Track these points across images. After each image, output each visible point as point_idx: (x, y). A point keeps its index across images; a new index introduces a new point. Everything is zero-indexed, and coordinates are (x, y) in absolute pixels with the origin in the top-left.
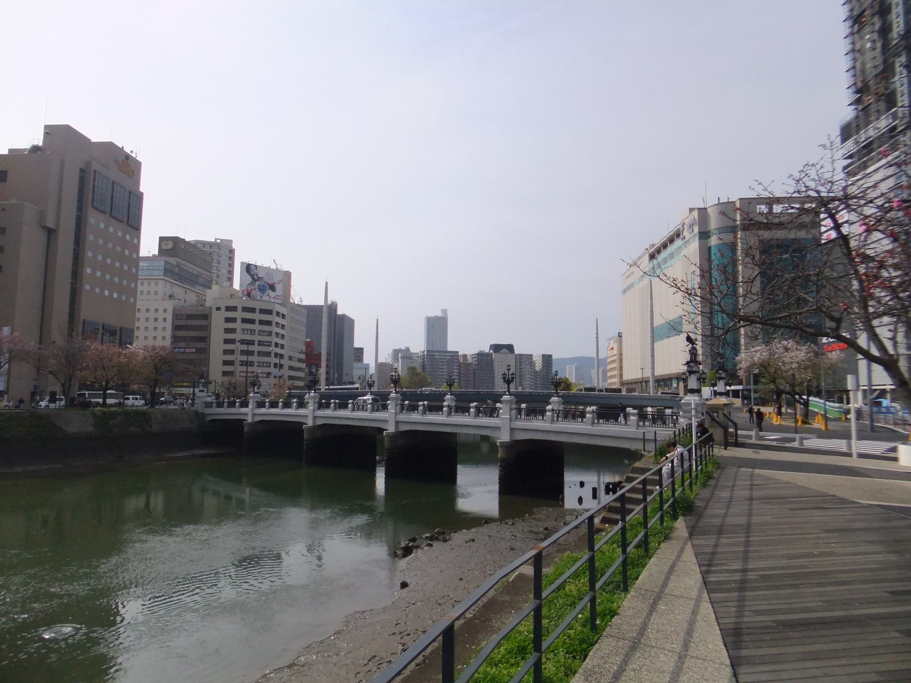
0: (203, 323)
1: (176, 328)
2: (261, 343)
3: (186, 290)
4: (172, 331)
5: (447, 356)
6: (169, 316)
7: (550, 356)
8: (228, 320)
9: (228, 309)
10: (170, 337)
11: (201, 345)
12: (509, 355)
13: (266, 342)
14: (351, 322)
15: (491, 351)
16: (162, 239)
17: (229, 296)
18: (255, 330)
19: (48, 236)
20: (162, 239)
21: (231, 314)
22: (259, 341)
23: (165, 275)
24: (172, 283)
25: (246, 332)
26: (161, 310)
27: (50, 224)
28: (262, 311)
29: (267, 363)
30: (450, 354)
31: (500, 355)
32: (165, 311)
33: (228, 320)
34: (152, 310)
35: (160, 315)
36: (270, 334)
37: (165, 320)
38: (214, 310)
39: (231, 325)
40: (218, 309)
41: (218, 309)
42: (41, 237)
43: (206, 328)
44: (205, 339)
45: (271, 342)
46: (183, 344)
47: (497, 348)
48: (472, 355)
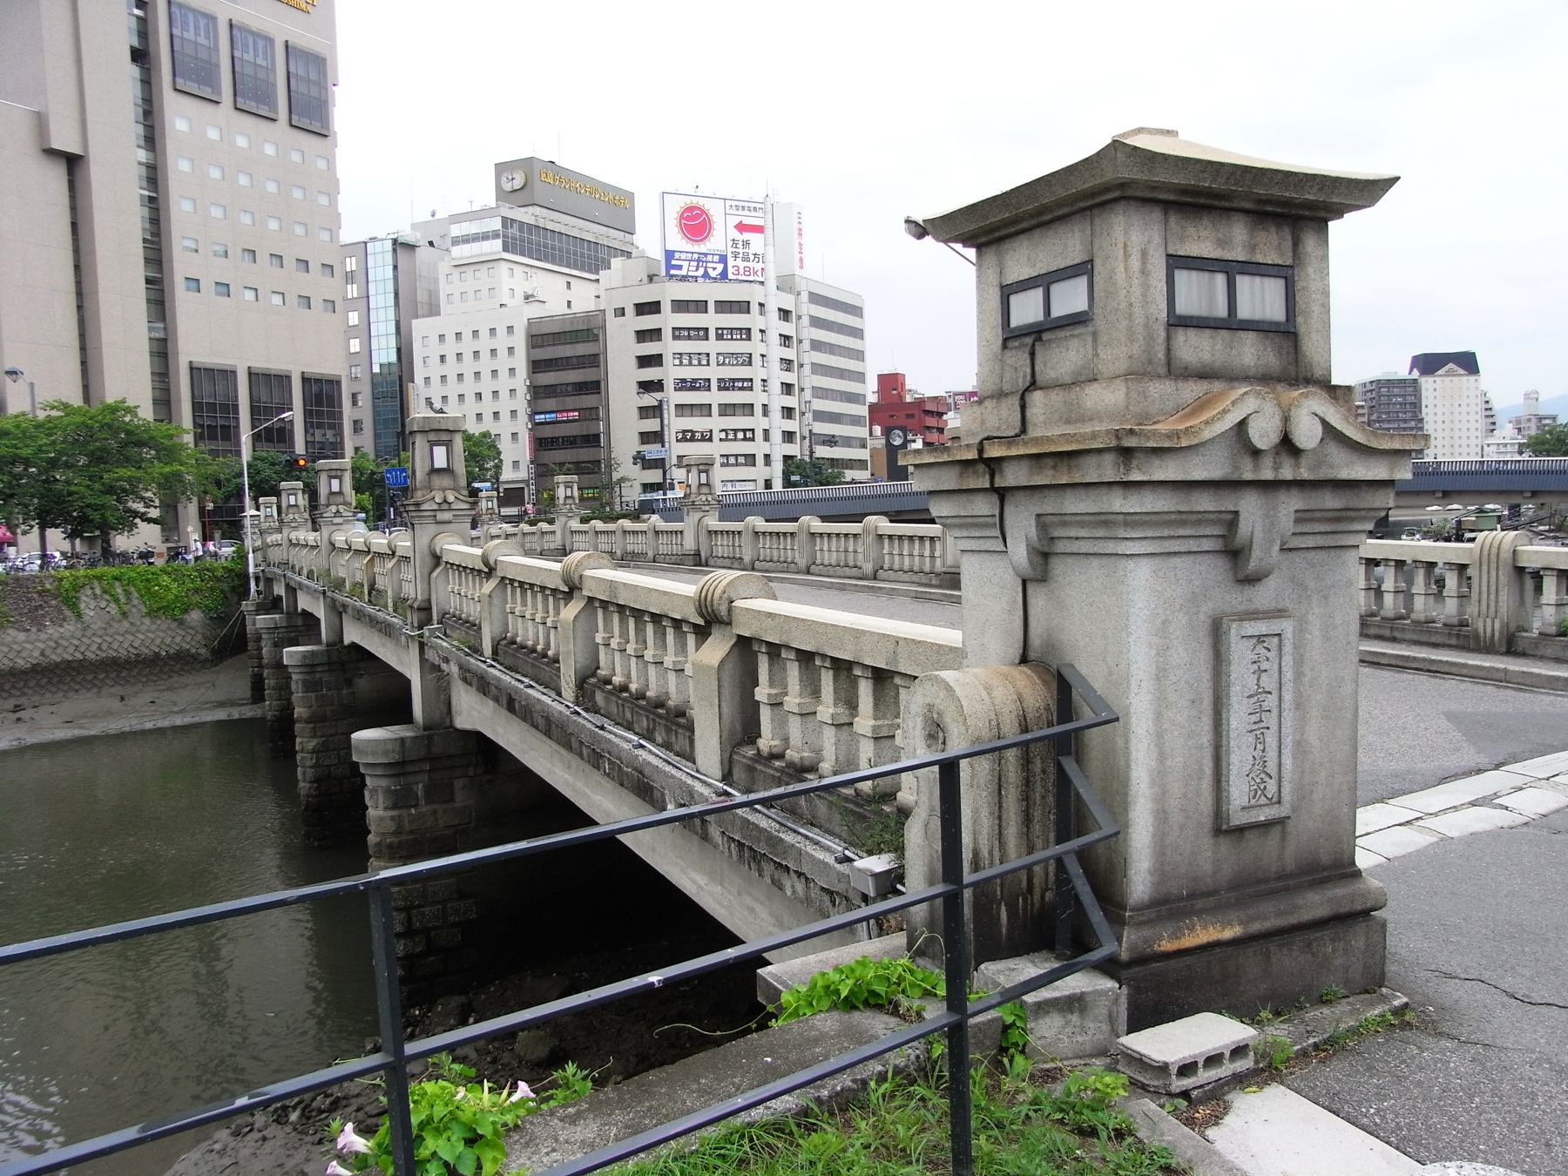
0: (581, 349)
1: (536, 366)
2: (726, 385)
3: (570, 279)
4: (529, 377)
6: (520, 341)
8: (643, 336)
9: (645, 308)
10: (525, 390)
11: (588, 401)
12: (1465, 379)
13: (739, 380)
14: (631, 196)
15: (1416, 374)
16: (501, 168)
17: (646, 279)
19: (69, 169)
20: (501, 168)
21: (648, 322)
22: (719, 380)
23: (505, 249)
24: (527, 265)
25: (695, 362)
27: (66, 142)
28: (725, 306)
29: (744, 431)
31: (1437, 379)
32: (510, 329)
33: (643, 336)
34: (1436, 402)
35: (502, 343)
37: (511, 350)
38: (610, 315)
39: (649, 348)
40: (621, 312)
41: (621, 312)
42: (56, 176)
43: (594, 361)
44: (595, 387)
45: (751, 380)
46: (551, 403)
47: (1429, 364)
48: (1365, 385)
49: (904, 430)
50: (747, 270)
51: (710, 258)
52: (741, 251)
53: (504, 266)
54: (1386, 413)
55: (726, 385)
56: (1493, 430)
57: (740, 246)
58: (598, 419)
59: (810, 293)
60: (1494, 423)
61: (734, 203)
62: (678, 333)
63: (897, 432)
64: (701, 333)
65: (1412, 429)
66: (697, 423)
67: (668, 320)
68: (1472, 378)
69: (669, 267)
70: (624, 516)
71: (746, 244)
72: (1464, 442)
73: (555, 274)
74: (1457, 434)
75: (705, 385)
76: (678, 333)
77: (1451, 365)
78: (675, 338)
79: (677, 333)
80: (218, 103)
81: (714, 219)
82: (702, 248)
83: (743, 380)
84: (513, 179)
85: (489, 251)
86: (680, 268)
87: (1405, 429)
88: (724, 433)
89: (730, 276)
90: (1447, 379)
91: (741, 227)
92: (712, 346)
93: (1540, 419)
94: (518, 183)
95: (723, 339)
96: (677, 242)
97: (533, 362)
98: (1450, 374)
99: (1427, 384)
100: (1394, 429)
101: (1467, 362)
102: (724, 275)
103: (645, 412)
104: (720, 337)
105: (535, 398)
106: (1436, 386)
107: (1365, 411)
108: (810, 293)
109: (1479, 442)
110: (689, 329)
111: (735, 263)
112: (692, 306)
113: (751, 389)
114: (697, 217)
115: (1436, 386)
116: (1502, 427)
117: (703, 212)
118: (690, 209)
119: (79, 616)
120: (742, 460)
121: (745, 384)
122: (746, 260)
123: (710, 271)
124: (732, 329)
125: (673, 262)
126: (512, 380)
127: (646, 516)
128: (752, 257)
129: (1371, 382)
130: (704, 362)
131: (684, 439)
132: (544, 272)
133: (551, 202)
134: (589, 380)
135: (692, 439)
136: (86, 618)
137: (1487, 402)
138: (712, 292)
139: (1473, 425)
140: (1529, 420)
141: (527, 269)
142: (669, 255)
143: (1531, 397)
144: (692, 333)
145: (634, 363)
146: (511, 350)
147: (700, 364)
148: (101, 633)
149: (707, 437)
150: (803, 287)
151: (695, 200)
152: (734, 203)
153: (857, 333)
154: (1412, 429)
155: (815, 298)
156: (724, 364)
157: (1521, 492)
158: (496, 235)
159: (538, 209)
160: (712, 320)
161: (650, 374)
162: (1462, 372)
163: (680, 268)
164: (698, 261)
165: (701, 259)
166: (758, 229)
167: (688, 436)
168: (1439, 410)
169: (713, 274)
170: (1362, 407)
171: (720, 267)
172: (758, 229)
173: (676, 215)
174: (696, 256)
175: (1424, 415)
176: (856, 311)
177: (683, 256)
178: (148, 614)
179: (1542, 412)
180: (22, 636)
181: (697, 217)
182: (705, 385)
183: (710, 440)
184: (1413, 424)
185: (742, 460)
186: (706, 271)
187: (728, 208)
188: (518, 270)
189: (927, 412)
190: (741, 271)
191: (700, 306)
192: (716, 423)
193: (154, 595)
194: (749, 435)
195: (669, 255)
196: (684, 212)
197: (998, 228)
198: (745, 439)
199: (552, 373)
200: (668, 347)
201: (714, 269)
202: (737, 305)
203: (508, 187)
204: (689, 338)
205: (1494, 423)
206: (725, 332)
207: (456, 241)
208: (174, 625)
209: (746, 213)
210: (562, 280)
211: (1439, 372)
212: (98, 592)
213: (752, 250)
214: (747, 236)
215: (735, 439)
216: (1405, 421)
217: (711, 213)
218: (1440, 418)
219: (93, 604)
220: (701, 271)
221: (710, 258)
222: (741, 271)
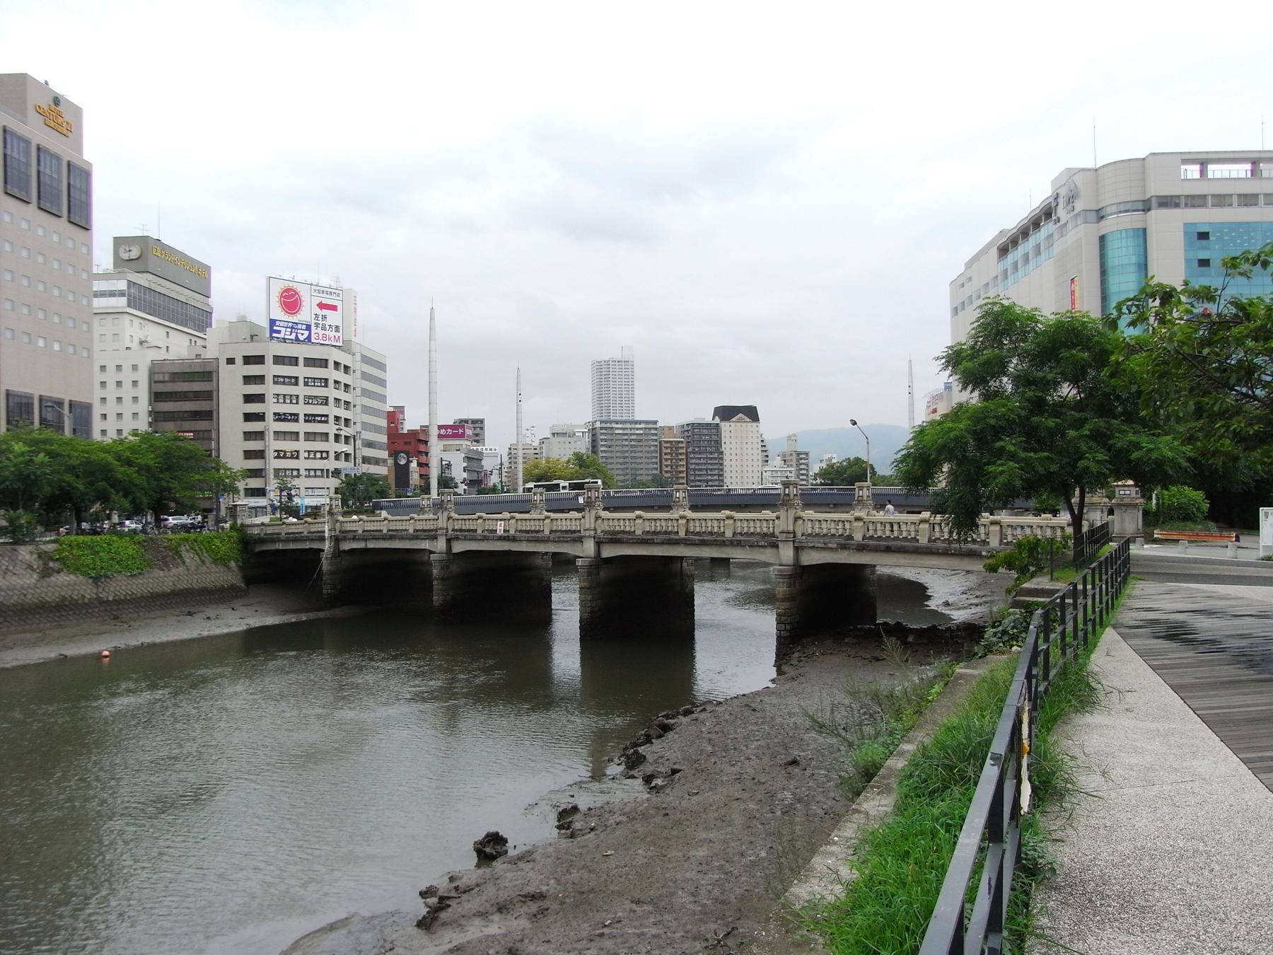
1: (157, 397)
2: (310, 418)
5: (637, 429)
7: (625, 366)
8: (248, 380)
9: (248, 360)
11: (202, 425)
13: (318, 415)
14: (208, 268)
15: (717, 420)
17: (249, 339)
18: (297, 397)
21: (254, 370)
22: (305, 415)
23: (129, 306)
25: (288, 401)
26: (111, 368)
28: (310, 362)
29: (322, 452)
30: (642, 426)
33: (248, 380)
35: (127, 376)
36: (325, 401)
38: (223, 362)
39: (254, 389)
40: (231, 361)
41: (231, 361)
43: (208, 395)
44: (208, 415)
45: (327, 416)
47: (726, 413)
49: (407, 453)
50: (324, 336)
51: (300, 326)
52: (320, 322)
53: (127, 318)
54: (699, 447)
55: (310, 418)
56: (767, 461)
57: (320, 319)
58: (211, 439)
59: (363, 356)
60: (767, 456)
61: (317, 288)
62: (278, 380)
63: (402, 454)
64: (293, 380)
65: (715, 459)
66: (288, 446)
67: (269, 369)
68: (755, 424)
69: (272, 331)
70: (573, 510)
71: (324, 317)
72: (750, 469)
73: (161, 327)
74: (745, 463)
75: (294, 418)
76: (278, 380)
77: (740, 415)
78: (275, 383)
79: (276, 379)
80: (88, 229)
81: (303, 299)
82: (295, 319)
83: (322, 416)
84: (130, 251)
85: (115, 305)
86: (279, 332)
87: (711, 459)
88: (307, 453)
89: (313, 340)
90: (739, 424)
91: (322, 306)
92: (301, 390)
93: (799, 454)
94: (134, 254)
95: (308, 386)
96: (278, 314)
97: (156, 393)
98: (739, 421)
99: (725, 426)
100: (704, 458)
101: (751, 413)
102: (309, 338)
103: (248, 436)
104: (306, 384)
105: (156, 421)
106: (731, 429)
107: (684, 445)
108: (363, 356)
109: (759, 469)
110: (284, 377)
111: (316, 331)
112: (287, 361)
113: (326, 422)
114: (292, 296)
115: (731, 429)
116: (774, 460)
117: (296, 293)
118: (288, 290)
119: (184, 562)
120: (319, 473)
121: (323, 419)
122: (324, 328)
123: (299, 336)
124: (315, 378)
125: (275, 328)
126: (135, 406)
127: (378, 512)
128: (328, 327)
129: (687, 425)
130: (294, 401)
131: (278, 457)
132: (152, 324)
133: (158, 271)
134: (203, 409)
135: (284, 457)
136: (187, 564)
137: (762, 441)
138: (302, 352)
139: (755, 458)
140: (791, 454)
141: (142, 321)
142: (273, 322)
143: (792, 438)
144: (287, 380)
145: (241, 399)
146: (135, 383)
147: (291, 403)
148: (195, 572)
149: (295, 455)
150: (356, 349)
151: (291, 284)
152: (317, 288)
153: (382, 383)
154: (715, 459)
155: (366, 360)
156: (308, 403)
157: (828, 505)
158: (122, 294)
159: (151, 276)
160: (301, 371)
161: (254, 408)
162: (748, 420)
163: (279, 332)
164: (292, 328)
165: (294, 327)
166: (334, 308)
167: (280, 455)
168: (733, 446)
169: (301, 338)
170: (682, 442)
171: (306, 333)
172: (334, 308)
173: (278, 294)
174: (290, 324)
175: (723, 449)
176: (382, 366)
177: (282, 324)
178: (213, 562)
179: (799, 450)
180: (161, 574)
181: (292, 296)
182: (294, 418)
183: (297, 458)
184: (716, 455)
185: (319, 473)
186: (297, 336)
187: (313, 291)
188: (136, 321)
189: (420, 441)
190: (321, 337)
191: (293, 361)
192: (302, 446)
193: (213, 551)
194: (324, 455)
195: (273, 322)
196: (284, 292)
197: (1245, 627)
198: (322, 458)
199: (172, 403)
200: (269, 389)
201: (302, 334)
202: (319, 362)
203: (125, 256)
204: (284, 383)
205: (767, 456)
206: (310, 380)
207: (97, 295)
208: (226, 569)
209: (325, 295)
210: (163, 331)
211: (734, 419)
212: (188, 548)
213: (328, 323)
214: (325, 312)
215: (315, 458)
216: (711, 453)
217: (301, 294)
218: (734, 452)
219: (187, 555)
220: (293, 336)
221: (300, 326)
222: (321, 337)
